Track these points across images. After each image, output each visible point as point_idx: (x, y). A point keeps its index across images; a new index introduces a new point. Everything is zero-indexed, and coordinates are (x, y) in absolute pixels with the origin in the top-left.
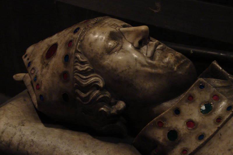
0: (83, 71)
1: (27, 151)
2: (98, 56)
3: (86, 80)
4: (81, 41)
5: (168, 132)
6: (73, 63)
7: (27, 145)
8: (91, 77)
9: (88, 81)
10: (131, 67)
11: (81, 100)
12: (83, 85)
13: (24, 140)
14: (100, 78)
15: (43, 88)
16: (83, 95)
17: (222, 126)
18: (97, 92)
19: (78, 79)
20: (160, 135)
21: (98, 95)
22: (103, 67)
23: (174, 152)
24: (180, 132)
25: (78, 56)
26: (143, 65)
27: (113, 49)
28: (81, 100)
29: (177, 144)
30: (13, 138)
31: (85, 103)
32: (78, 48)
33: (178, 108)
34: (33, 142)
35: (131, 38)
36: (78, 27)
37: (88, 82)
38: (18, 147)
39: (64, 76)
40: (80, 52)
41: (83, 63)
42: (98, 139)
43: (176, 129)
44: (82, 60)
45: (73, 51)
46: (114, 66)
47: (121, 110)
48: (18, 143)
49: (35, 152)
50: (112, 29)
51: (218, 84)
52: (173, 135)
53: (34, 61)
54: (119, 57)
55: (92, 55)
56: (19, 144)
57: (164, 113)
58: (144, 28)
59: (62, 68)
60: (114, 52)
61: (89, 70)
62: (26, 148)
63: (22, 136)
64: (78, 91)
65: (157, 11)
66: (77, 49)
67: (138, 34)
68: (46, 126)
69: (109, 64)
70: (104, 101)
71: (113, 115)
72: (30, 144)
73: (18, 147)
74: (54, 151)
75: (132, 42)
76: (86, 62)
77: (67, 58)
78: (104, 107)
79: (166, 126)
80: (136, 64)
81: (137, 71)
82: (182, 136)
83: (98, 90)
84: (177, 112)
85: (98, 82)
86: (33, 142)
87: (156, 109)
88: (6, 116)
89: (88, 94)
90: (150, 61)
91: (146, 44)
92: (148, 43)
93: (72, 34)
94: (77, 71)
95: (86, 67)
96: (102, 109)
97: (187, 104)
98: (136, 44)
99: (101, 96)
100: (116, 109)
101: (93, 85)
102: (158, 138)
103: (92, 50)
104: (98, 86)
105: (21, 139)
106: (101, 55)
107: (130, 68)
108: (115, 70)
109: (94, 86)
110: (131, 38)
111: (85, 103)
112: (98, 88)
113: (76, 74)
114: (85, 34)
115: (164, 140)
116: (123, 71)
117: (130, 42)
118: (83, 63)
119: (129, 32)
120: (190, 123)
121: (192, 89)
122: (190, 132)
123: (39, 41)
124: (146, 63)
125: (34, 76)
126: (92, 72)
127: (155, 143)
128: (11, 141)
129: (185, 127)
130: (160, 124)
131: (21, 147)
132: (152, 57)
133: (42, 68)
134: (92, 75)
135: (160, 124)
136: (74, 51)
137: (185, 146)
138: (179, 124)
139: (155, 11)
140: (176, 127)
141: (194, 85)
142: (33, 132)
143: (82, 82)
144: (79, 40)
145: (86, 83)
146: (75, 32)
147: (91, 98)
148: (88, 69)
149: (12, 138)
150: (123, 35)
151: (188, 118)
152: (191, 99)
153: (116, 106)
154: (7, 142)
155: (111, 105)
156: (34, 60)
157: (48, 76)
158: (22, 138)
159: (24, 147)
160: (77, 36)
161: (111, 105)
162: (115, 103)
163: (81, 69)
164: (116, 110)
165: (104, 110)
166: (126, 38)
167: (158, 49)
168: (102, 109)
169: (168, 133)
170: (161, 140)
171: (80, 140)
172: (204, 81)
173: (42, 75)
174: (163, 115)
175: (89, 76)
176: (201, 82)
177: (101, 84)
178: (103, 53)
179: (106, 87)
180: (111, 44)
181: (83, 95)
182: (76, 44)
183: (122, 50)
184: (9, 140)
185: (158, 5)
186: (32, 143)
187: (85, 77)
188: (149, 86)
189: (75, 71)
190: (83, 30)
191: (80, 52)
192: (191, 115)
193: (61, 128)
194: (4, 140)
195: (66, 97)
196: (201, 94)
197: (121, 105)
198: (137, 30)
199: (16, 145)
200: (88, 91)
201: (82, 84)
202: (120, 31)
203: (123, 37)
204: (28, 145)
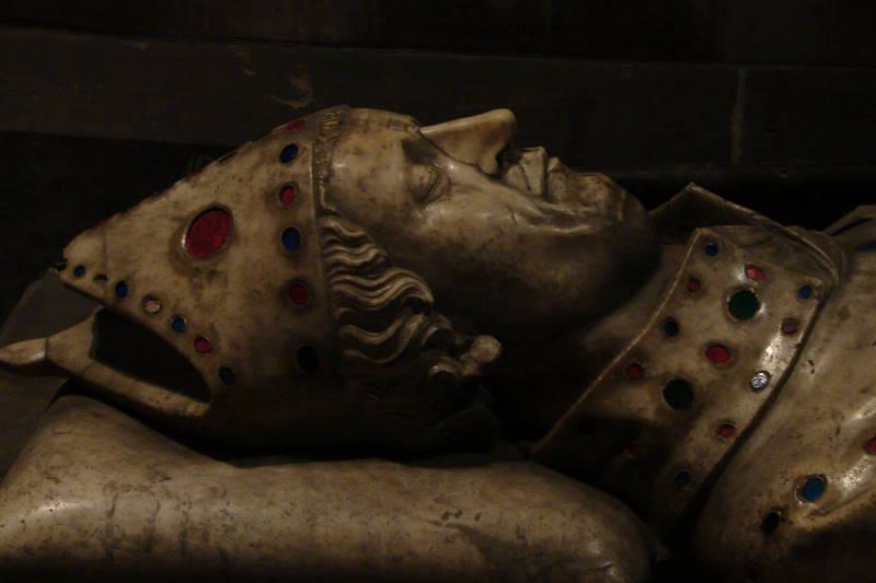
0: (365, 264)
1: (219, 548)
2: (397, 215)
3: (379, 292)
4: (327, 180)
5: (662, 388)
6: (318, 248)
7: (213, 531)
8: (392, 280)
9: (387, 290)
10: (504, 230)
11: (364, 357)
12: (373, 306)
13: (117, 534)
14: (411, 276)
15: (224, 344)
16: (375, 338)
17: (805, 340)
18: (419, 319)
19: (350, 291)
20: (643, 402)
21: (422, 329)
22: (419, 245)
23: (691, 439)
24: (696, 380)
25: (333, 224)
26: (534, 220)
27: (432, 187)
28: (364, 357)
29: (697, 415)
30: (154, 521)
31: (381, 361)
32: (326, 200)
33: (670, 318)
34: (232, 518)
35: (467, 148)
36: (288, 143)
37: (387, 296)
38: (183, 543)
39: (296, 293)
40: (334, 214)
41: (354, 243)
42: (429, 466)
43: (684, 377)
44: (350, 234)
45: (306, 213)
46: (455, 235)
47: (494, 361)
48: (178, 532)
49: (251, 545)
50: (403, 135)
51: (744, 238)
52: (680, 392)
53: (138, 276)
54: (438, 216)
55: (377, 215)
56: (184, 534)
57: (638, 339)
58: (501, 115)
59: (282, 272)
60: (439, 197)
61: (381, 260)
62: (212, 538)
63: (185, 508)
64: (352, 330)
65: (304, 105)
66: (324, 204)
67: (489, 135)
68: (239, 465)
69: (435, 231)
70: (441, 344)
71: (471, 382)
72: (223, 526)
73: (183, 543)
74: (313, 525)
75: (472, 161)
76: (363, 237)
77: (291, 239)
78: (444, 362)
79: (654, 373)
80: (546, 175)
81: (522, 238)
82: (705, 389)
83: (417, 313)
84: (671, 328)
85: (413, 289)
86: (232, 518)
87: (592, 339)
88: (87, 467)
89: (391, 330)
90: (546, 205)
91: (515, 161)
92: (520, 158)
93: (278, 166)
94: (340, 268)
95: (370, 253)
96: (436, 368)
97: (690, 302)
98: (489, 163)
99: (433, 330)
100: (476, 361)
101: (403, 301)
102: (640, 410)
103: (372, 200)
104: (421, 300)
105: (187, 519)
106: (403, 211)
107: (502, 232)
108: (460, 246)
109: (407, 304)
110: (467, 148)
111: (381, 361)
112: (418, 306)
113: (340, 278)
114: (328, 159)
115: (660, 410)
116: (484, 246)
117: (468, 162)
118: (354, 243)
119: (456, 136)
120: (717, 352)
121: (691, 261)
122: (725, 376)
123: (109, 215)
124: (537, 213)
125: (165, 318)
126: (387, 265)
127: (631, 428)
128: (153, 530)
129: (705, 365)
130: (635, 371)
131: (194, 542)
132: (546, 195)
133: (197, 289)
134: (391, 273)
135: (635, 371)
136: (312, 213)
137: (723, 416)
138: (686, 361)
139: (296, 105)
140: (680, 371)
141: (690, 249)
142: (213, 490)
143: (366, 299)
144: (316, 179)
145: (381, 300)
146: (288, 155)
147: (406, 341)
148: (377, 256)
149: (151, 521)
150: (438, 148)
151: (702, 339)
152: (695, 286)
153: (475, 354)
154: (139, 536)
155: (455, 352)
156: (134, 272)
157: (233, 304)
158: (185, 513)
159: (205, 537)
160: (301, 169)
161: (455, 352)
162: (468, 346)
163: (358, 261)
164: (476, 365)
165: (448, 370)
166: (451, 154)
167: (553, 171)
168: (436, 368)
169: (665, 392)
170: (650, 414)
171: (375, 478)
172: (715, 235)
173: (207, 309)
174: (638, 343)
175: (382, 280)
176: (707, 238)
177: (428, 296)
178: (407, 204)
179: (443, 304)
180: (421, 174)
181: (375, 338)
182: (311, 191)
183: (454, 188)
184: (145, 530)
185: (301, 84)
186: (228, 522)
187: (375, 283)
188: (564, 273)
189: (334, 271)
190: (314, 150)
191: (334, 214)
192: (708, 330)
193: (290, 462)
194: (124, 535)
195: (308, 360)
196: (715, 270)
197: (488, 347)
198: (487, 124)
199: (175, 539)
200: (391, 322)
201: (367, 305)
202: (423, 136)
203: (436, 151)
204: (217, 530)
